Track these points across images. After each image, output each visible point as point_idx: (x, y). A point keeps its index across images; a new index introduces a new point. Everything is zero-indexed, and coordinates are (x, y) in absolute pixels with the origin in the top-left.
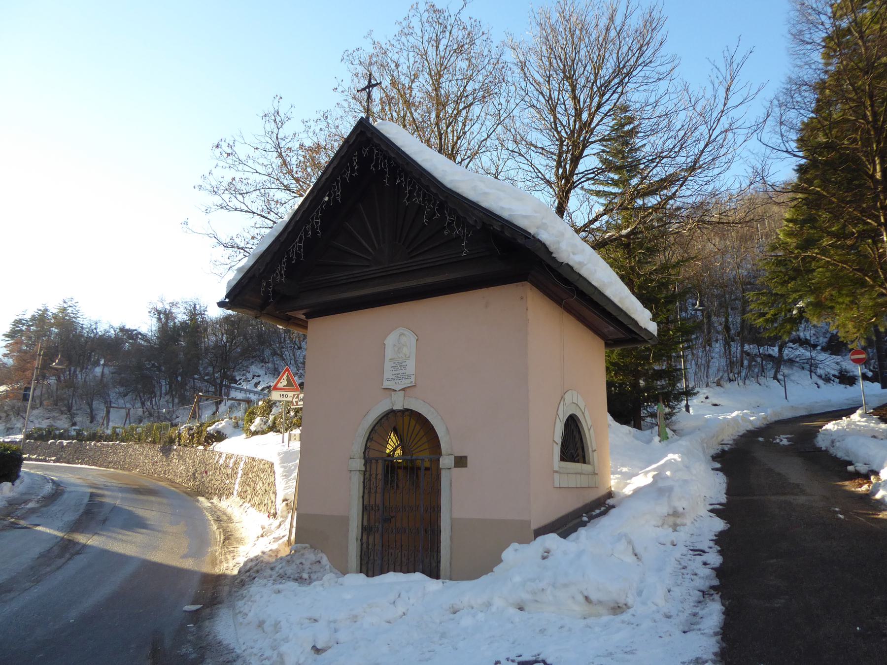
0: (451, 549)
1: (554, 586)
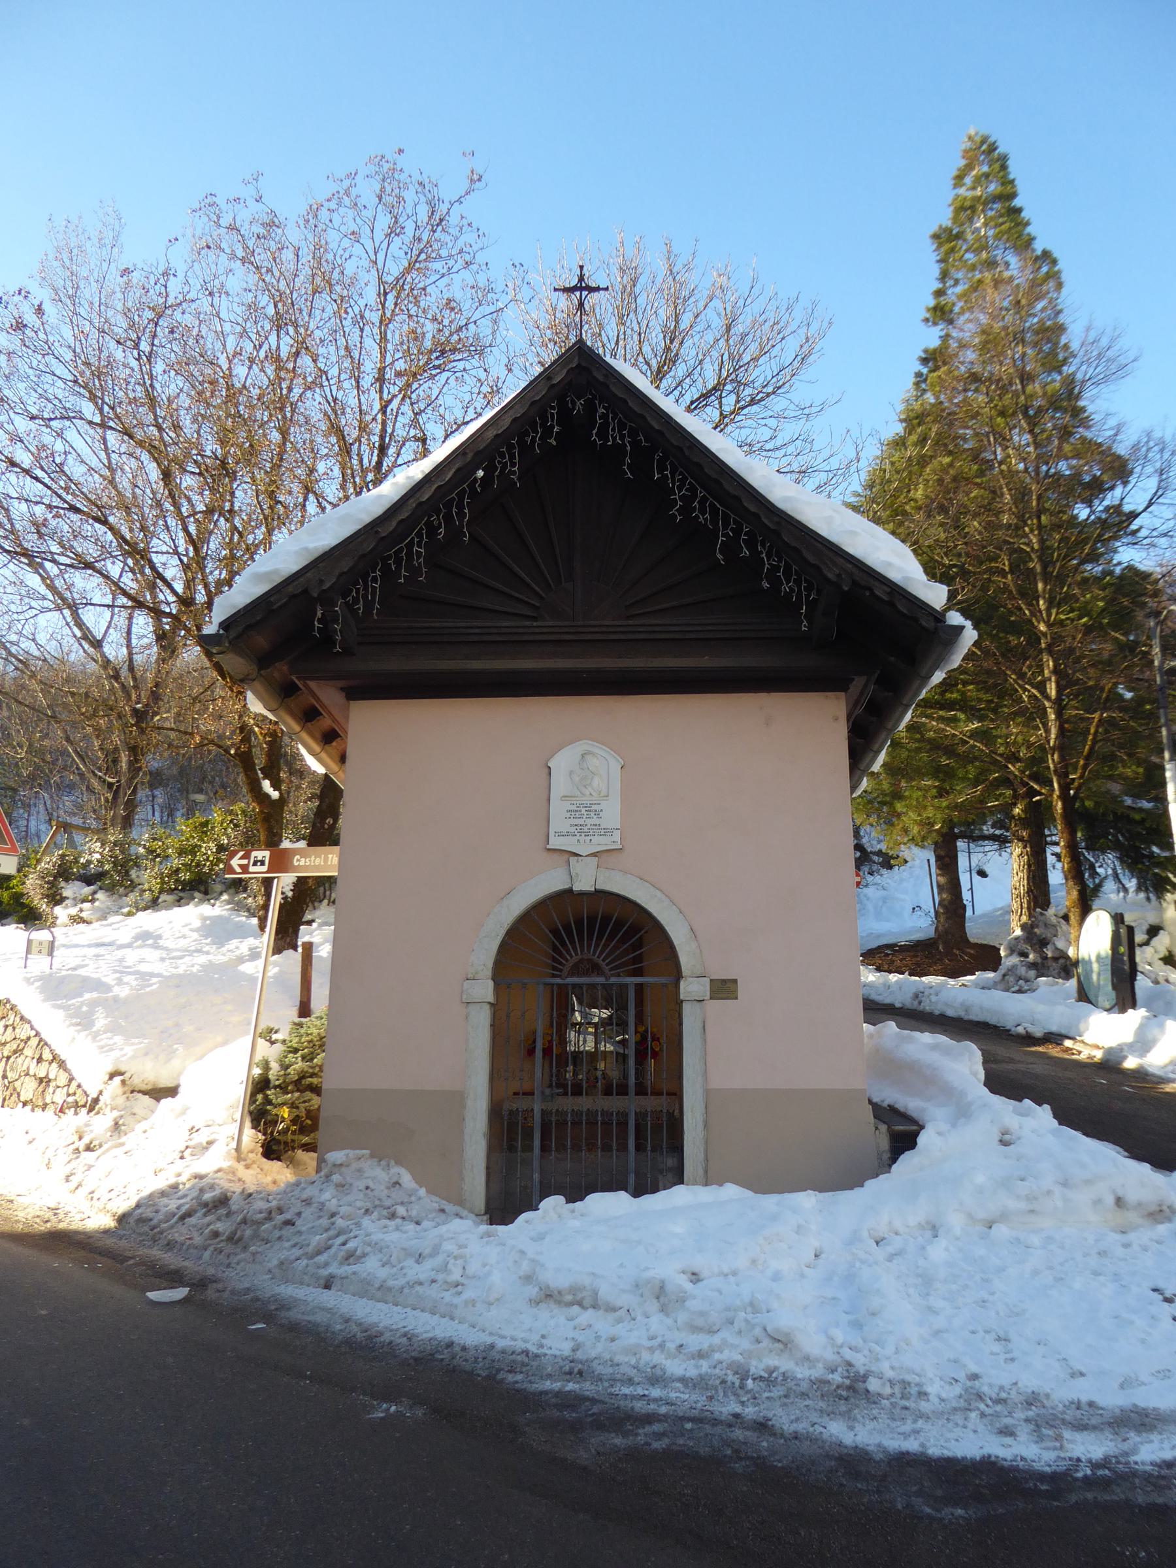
0: (706, 1143)
1: (1065, 1184)
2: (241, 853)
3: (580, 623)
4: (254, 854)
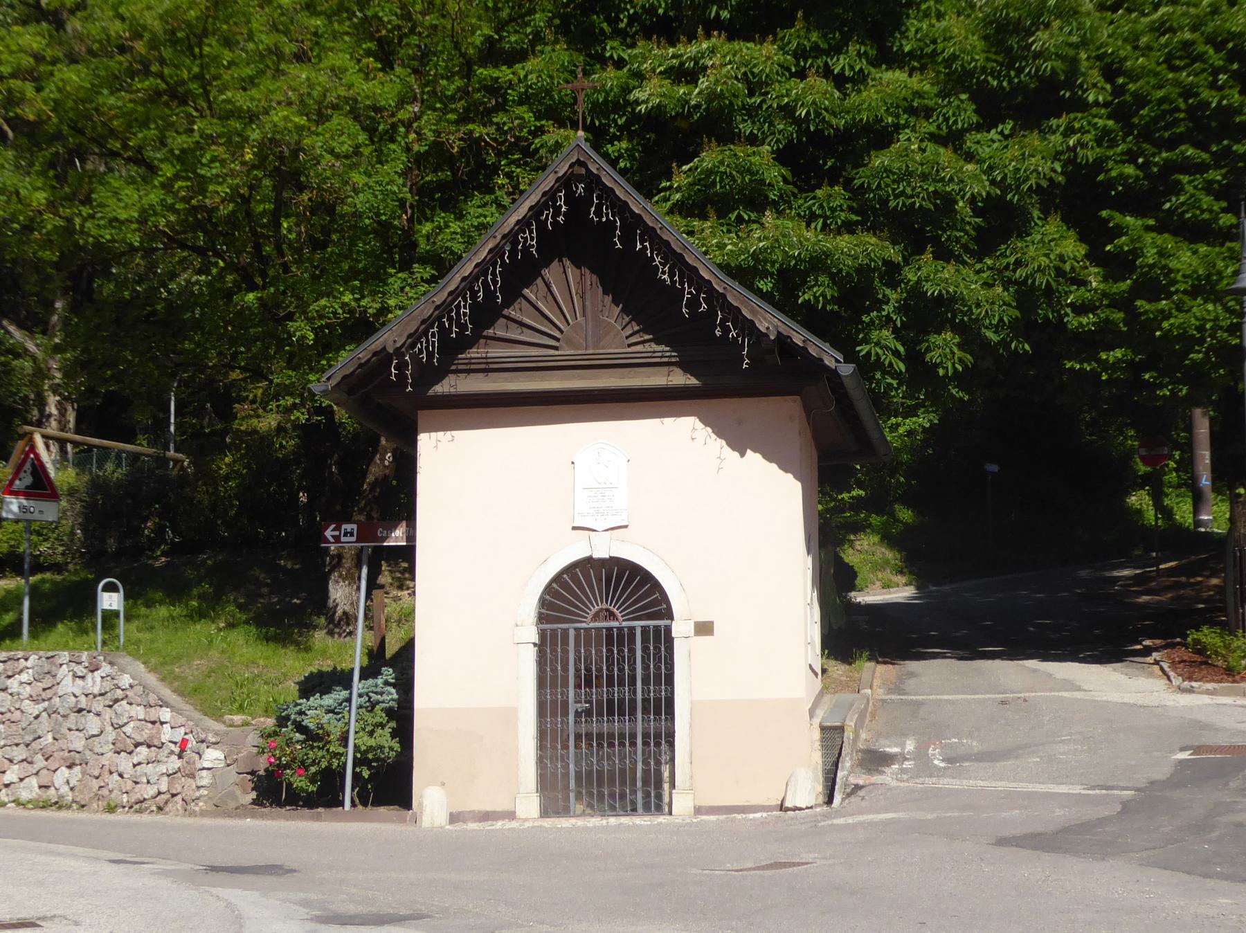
2: (333, 526)
3: (591, 352)
4: (344, 526)
